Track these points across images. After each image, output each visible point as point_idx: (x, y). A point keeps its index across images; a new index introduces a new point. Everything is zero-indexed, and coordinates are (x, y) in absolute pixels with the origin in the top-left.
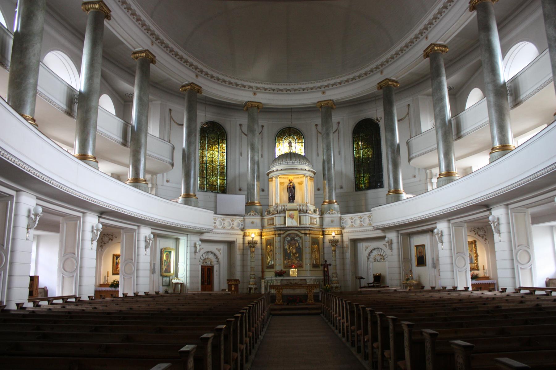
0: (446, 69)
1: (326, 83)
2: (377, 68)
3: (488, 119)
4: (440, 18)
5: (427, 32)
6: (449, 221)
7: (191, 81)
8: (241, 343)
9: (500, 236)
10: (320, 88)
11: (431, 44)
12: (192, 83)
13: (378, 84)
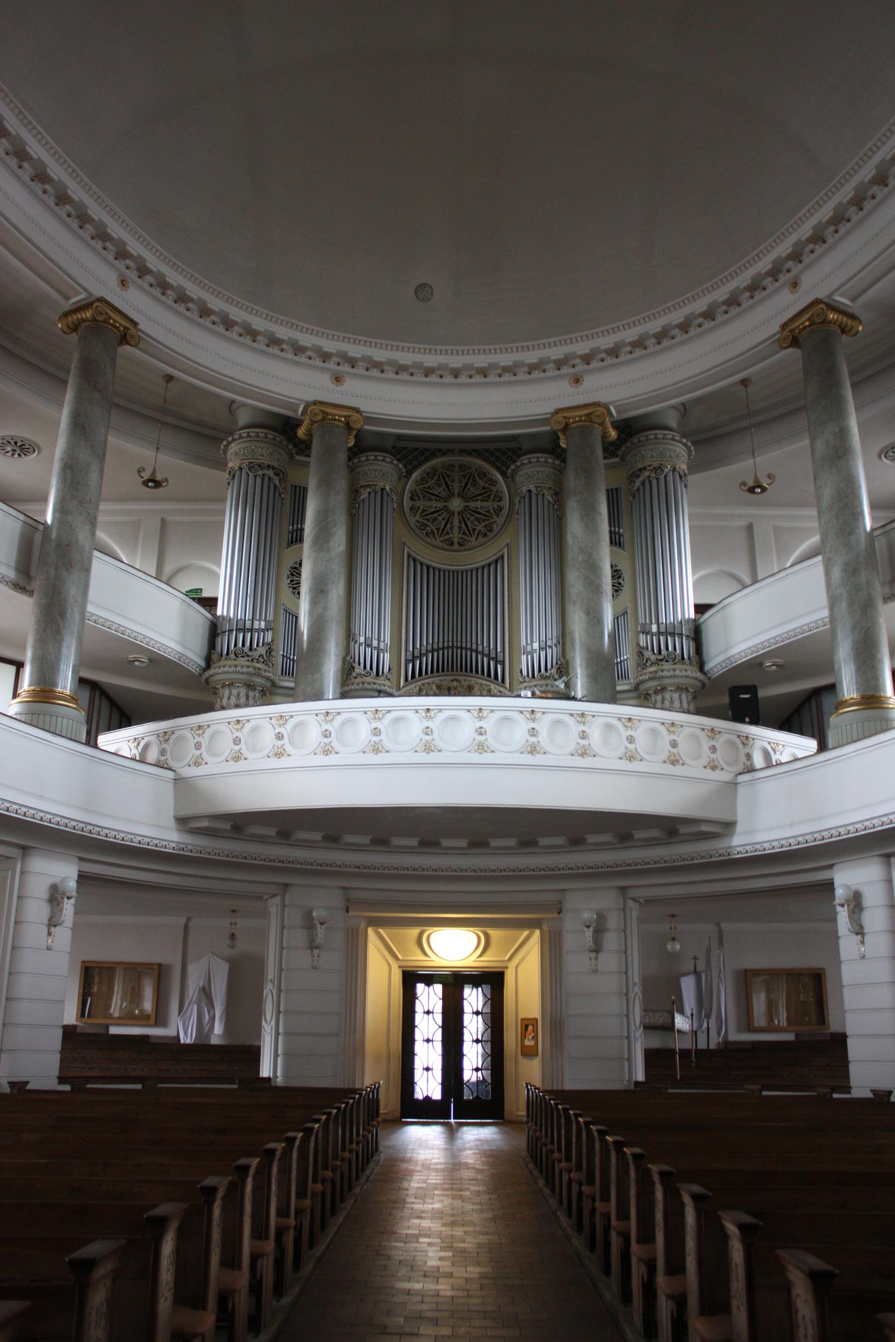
0: (854, 386)
1: (582, 348)
2: (775, 272)
3: (825, 613)
4: (770, 289)
5: (796, 268)
6: (623, 890)
7: (98, 292)
8: (231, 1261)
9: (862, 942)
10: (559, 364)
11: (817, 302)
12: (101, 300)
13: (784, 326)
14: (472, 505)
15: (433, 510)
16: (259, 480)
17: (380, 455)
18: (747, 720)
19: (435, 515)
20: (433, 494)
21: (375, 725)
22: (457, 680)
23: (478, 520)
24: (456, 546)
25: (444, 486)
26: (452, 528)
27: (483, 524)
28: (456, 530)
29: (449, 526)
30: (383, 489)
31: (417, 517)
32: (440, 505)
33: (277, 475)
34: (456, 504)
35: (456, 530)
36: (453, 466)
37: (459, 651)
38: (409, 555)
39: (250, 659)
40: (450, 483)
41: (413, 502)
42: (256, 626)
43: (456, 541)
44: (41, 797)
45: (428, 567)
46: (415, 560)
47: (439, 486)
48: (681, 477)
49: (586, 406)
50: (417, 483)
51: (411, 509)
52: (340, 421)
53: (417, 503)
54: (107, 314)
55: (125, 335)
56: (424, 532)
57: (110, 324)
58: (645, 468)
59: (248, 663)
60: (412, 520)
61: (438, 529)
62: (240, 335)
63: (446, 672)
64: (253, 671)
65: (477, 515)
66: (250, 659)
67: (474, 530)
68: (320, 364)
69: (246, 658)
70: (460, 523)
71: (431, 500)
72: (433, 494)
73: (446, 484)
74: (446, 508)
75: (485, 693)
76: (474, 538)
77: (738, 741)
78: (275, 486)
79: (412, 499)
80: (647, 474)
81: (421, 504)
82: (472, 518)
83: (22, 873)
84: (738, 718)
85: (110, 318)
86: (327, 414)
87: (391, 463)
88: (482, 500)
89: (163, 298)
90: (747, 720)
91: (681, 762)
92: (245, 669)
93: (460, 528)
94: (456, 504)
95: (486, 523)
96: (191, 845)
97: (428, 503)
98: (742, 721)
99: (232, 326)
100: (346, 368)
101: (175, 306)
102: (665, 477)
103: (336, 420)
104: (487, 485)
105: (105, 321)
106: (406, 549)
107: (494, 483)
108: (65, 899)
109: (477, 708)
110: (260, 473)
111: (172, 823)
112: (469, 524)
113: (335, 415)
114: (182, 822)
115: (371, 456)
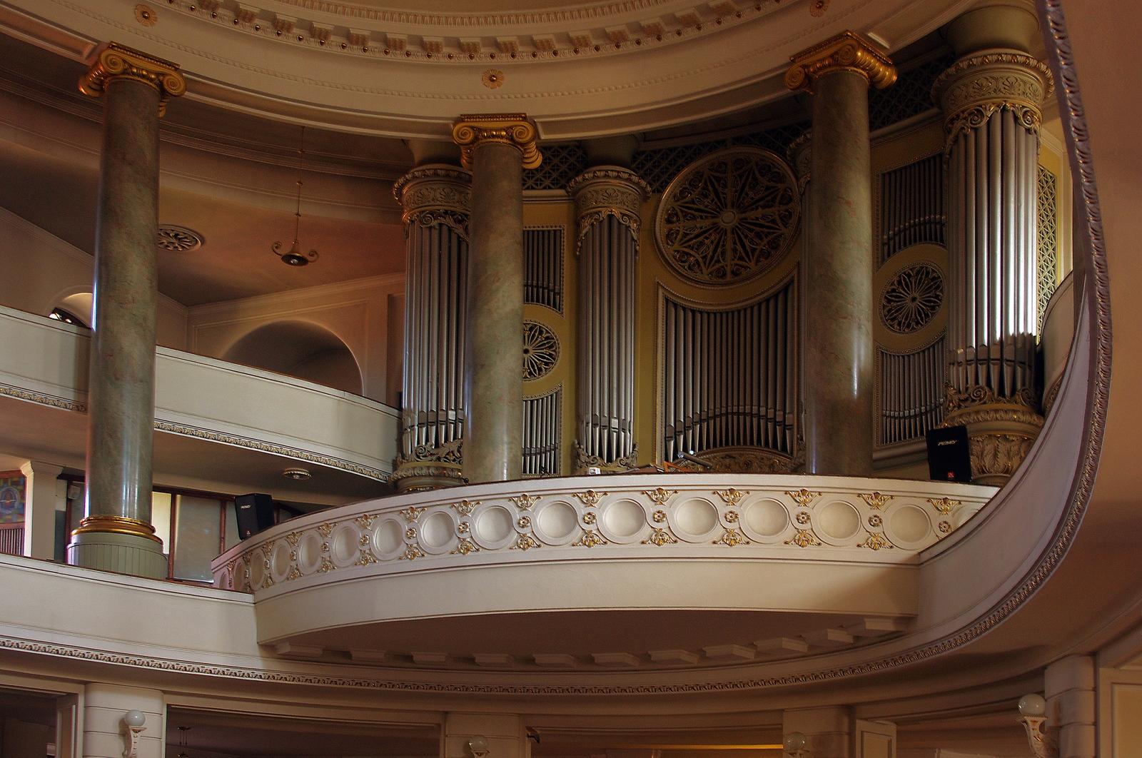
14: (751, 215)
15: (697, 232)
16: (435, 233)
17: (613, 169)
18: (951, 475)
19: (700, 239)
20: (697, 210)
21: (807, 526)
22: (730, 456)
23: (758, 235)
24: (729, 278)
25: (712, 195)
26: (723, 253)
27: (766, 241)
28: (729, 254)
29: (720, 250)
30: (611, 217)
31: (676, 247)
32: (706, 223)
33: (459, 222)
34: (729, 218)
35: (729, 254)
36: (725, 164)
37: (735, 417)
38: (667, 300)
39: (434, 458)
40: (720, 190)
41: (670, 226)
42: (907, 414)
43: (728, 269)
44: (52, 630)
45: (693, 312)
46: (676, 305)
47: (706, 196)
48: (1016, 118)
49: (828, 42)
50: (676, 198)
51: (668, 236)
52: (502, 137)
53: (675, 227)
54: (124, 61)
55: (161, 85)
56: (686, 265)
57: (134, 74)
58: (958, 116)
59: (432, 463)
60: (669, 251)
61: (704, 258)
62: (343, 47)
63: (731, 446)
64: (436, 472)
65: (757, 229)
66: (434, 458)
67: (754, 250)
68: (614, 51)
69: (429, 458)
70: (735, 243)
71: (694, 218)
72: (697, 210)
73: (716, 191)
74: (715, 227)
75: (767, 469)
76: (753, 263)
77: (929, 507)
78: (459, 237)
79: (669, 221)
80: (958, 124)
81: (681, 226)
82: (751, 235)
83: (86, 707)
84: (938, 474)
85: (131, 66)
86: (480, 130)
87: (629, 180)
88: (764, 207)
89: (215, 21)
90: (951, 475)
91: (816, 540)
92: (424, 472)
93: (735, 250)
94: (729, 218)
95: (770, 237)
96: (286, 673)
97: (690, 224)
98: (944, 479)
99: (326, 38)
100: (504, 59)
101: (237, 28)
102: (989, 123)
103: (494, 136)
104: (772, 184)
105: (124, 72)
106: (661, 291)
107: (780, 178)
108: (132, 733)
109: (872, 492)
110: (434, 223)
111: (256, 650)
112: (747, 243)
113: (492, 130)
114: (269, 648)
115: (600, 170)
